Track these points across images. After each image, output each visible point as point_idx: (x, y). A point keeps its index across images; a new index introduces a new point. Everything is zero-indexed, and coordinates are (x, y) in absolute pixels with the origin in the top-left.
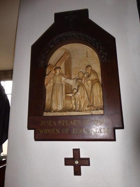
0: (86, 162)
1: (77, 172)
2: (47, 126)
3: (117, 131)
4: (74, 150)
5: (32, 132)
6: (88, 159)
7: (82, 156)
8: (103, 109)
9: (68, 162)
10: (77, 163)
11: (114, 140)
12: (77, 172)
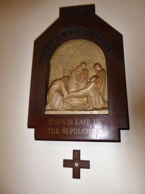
0: (86, 165)
1: (76, 175)
2: (46, 126)
3: (122, 131)
4: (74, 151)
5: (33, 130)
7: (82, 158)
8: (109, 109)
9: (67, 163)
10: (77, 165)
11: (119, 141)
12: (76, 175)
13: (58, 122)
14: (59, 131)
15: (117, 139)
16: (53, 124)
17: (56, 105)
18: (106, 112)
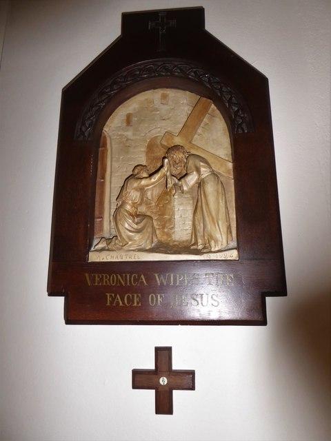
0: (187, 380)
1: (164, 406)
2: (93, 290)
5: (60, 301)
6: (192, 373)
9: (141, 379)
10: (163, 381)
12: (164, 406)
14: (140, 301)
15: (258, 319)
17: (120, 242)
18: (233, 255)
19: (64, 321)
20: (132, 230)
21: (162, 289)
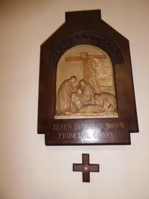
0: (96, 168)
1: (86, 179)
2: (55, 130)
5: (43, 136)
6: (98, 165)
9: (76, 168)
10: (86, 169)
12: (86, 179)
13: (64, 127)
16: (58, 129)
19: (98, 173)
20: (68, 92)
21: (72, 132)
